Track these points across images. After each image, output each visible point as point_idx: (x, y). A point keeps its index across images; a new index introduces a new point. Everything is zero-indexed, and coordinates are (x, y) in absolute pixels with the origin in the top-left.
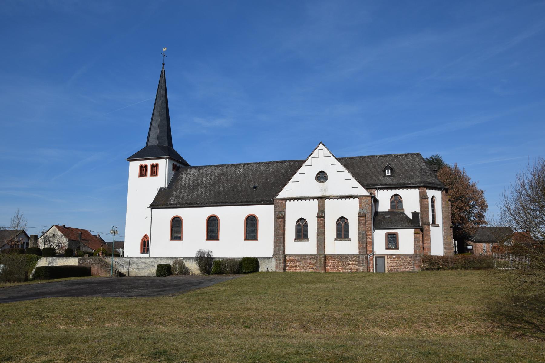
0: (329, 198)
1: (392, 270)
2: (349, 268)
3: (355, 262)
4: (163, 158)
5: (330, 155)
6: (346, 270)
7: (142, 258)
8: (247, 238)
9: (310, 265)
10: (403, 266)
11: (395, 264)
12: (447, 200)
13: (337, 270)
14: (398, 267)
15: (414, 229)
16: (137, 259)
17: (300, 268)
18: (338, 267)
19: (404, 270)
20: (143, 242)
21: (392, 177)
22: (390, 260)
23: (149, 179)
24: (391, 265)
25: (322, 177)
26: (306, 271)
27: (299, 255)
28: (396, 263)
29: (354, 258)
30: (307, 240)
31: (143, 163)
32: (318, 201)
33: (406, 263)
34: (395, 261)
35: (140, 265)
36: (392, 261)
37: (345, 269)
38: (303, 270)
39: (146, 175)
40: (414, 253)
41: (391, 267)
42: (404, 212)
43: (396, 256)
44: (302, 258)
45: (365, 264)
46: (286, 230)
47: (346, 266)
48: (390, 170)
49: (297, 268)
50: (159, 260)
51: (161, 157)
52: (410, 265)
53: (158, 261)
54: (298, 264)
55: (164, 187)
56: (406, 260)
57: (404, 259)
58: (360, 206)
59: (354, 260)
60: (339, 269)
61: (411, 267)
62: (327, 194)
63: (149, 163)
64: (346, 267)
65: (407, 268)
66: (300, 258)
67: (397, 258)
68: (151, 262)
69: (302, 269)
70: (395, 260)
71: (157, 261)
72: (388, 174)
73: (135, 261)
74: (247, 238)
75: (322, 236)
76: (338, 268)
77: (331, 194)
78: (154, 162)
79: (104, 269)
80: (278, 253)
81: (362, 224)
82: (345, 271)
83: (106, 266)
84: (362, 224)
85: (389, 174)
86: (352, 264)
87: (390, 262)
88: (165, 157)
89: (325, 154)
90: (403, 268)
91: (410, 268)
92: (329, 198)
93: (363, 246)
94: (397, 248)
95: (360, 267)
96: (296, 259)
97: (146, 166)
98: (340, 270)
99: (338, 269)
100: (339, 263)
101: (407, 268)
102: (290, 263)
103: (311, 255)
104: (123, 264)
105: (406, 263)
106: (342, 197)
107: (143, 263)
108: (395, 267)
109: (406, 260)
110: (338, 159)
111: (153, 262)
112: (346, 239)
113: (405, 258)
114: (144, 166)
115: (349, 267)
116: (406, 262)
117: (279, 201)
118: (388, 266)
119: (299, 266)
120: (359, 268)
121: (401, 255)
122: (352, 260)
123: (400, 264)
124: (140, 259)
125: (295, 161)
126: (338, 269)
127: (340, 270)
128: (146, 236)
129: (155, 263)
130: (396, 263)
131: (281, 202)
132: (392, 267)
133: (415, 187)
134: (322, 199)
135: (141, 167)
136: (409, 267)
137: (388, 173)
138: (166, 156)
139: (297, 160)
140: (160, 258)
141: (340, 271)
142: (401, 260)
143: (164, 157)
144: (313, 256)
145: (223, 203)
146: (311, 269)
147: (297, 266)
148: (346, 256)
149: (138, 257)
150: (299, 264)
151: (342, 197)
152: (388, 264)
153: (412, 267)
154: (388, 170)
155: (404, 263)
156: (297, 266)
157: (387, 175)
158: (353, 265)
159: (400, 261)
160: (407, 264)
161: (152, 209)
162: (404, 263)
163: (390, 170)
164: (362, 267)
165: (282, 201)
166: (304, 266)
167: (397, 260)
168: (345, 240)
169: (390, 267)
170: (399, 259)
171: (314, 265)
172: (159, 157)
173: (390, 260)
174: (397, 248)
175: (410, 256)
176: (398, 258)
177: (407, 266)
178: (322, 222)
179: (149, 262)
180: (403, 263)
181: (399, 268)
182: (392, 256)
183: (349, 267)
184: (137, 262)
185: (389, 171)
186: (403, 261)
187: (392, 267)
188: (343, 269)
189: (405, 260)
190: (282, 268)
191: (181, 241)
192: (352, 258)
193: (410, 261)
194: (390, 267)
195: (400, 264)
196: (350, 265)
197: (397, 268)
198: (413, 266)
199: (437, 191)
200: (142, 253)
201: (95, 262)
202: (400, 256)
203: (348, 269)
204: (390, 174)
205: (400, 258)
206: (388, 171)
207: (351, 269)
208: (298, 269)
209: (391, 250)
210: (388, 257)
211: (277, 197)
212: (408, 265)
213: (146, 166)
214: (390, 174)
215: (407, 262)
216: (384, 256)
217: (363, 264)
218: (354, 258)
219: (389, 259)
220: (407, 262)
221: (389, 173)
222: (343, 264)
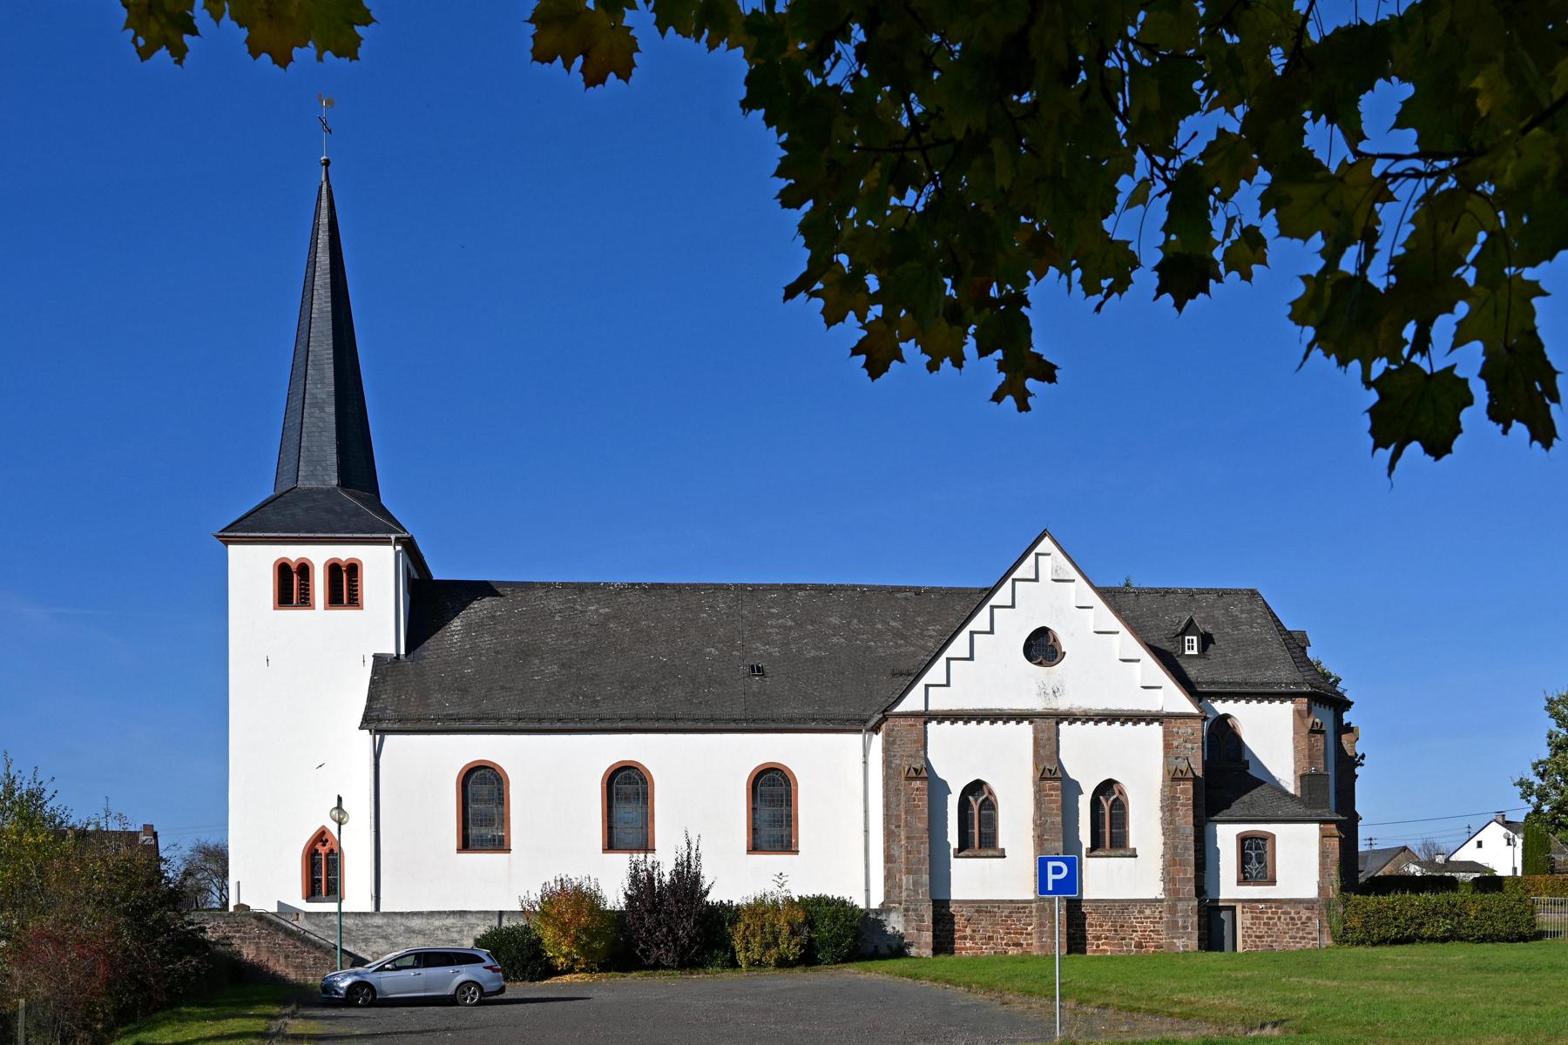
0: (1071, 717)
1: (1257, 946)
2: (1133, 942)
3: (1151, 922)
4: (386, 542)
5: (1074, 574)
6: (1125, 948)
7: (408, 913)
8: (466, 844)
9: (1010, 933)
10: (1287, 936)
11: (1264, 929)
12: (1307, 732)
13: (1094, 947)
14: (1273, 936)
15: (1321, 822)
16: (385, 920)
17: (977, 944)
18: (1098, 938)
19: (1291, 947)
20: (309, 855)
21: (1203, 662)
22: (1249, 915)
23: (319, 617)
24: (1254, 932)
25: (1041, 647)
26: (995, 953)
27: (973, 901)
28: (1268, 924)
29: (1148, 912)
30: (997, 854)
31: (294, 553)
32: (1031, 726)
33: (1297, 924)
34: (1265, 921)
35: (400, 940)
36: (1257, 918)
37: (1121, 946)
38: (987, 950)
39: (305, 601)
40: (1319, 894)
41: (1254, 938)
42: (1248, 771)
43: (1268, 905)
44: (982, 911)
45: (1192, 929)
46: (1158, 814)
47: (1122, 935)
48: (1195, 638)
49: (968, 945)
50: (479, 922)
51: (266, 535)
52: (1308, 930)
53: (472, 927)
54: (968, 931)
55: (391, 650)
56: (1296, 916)
57: (1289, 913)
58: (1167, 746)
59: (1149, 918)
60: (1103, 944)
61: (1310, 936)
62: (1062, 704)
63: (319, 556)
64: (1123, 939)
65: (1298, 940)
66: (977, 911)
67: (1269, 911)
68: (448, 929)
69: (984, 947)
70: (1265, 916)
71: (469, 925)
72: (1189, 649)
73: (377, 927)
74: (466, 844)
75: (1058, 840)
76: (1100, 942)
77: (1093, 708)
78: (344, 553)
79: (287, 957)
80: (912, 893)
81: (1182, 805)
82: (1120, 951)
83: (296, 947)
84: (1182, 805)
85: (1193, 649)
86: (1140, 927)
87: (1252, 924)
88: (393, 537)
89: (1056, 571)
90: (1288, 939)
91: (1309, 939)
92: (1071, 717)
93: (1185, 872)
94: (1273, 882)
95: (1179, 938)
96: (963, 915)
97: (304, 569)
98: (1105, 947)
99: (1098, 946)
100: (1101, 926)
101: (1298, 940)
102: (944, 927)
103: (1011, 901)
104: (329, 936)
105: (1297, 924)
106: (1111, 717)
107: (414, 932)
108: (1266, 939)
109: (1296, 916)
110: (1107, 594)
111: (454, 930)
112: (990, 852)
113: (1293, 912)
114: (294, 568)
115: (1131, 939)
116: (1296, 922)
117: (902, 721)
118: (1244, 936)
119: (972, 938)
120: (1175, 940)
121: (1281, 900)
122: (1142, 916)
123: (1278, 929)
124: (399, 920)
125: (861, 586)
126: (1098, 946)
127: (1105, 947)
128: (321, 836)
129: (460, 931)
130: (1268, 924)
131: (910, 725)
132: (1257, 937)
133: (1283, 696)
134: (1047, 723)
135: (283, 570)
136: (1304, 938)
137: (1189, 646)
138: (399, 535)
139: (870, 586)
140: (482, 916)
141: (1106, 951)
142: (1283, 917)
143: (389, 535)
144: (1021, 905)
145: (852, 724)
146: (1014, 945)
147: (965, 938)
148: (1123, 906)
149: (487, 912)
150: (974, 931)
151: (1111, 717)
152: (1243, 928)
153: (1317, 937)
154: (1190, 638)
155: (1290, 926)
156: (965, 938)
157: (1187, 652)
158: (1145, 931)
159: (1279, 918)
160: (1298, 929)
161: (383, 732)
162: (1290, 926)
163: (1195, 638)
164: (1183, 938)
165: (911, 721)
166: (990, 938)
167: (1270, 915)
168: (1113, 854)
169: (1250, 936)
170: (1276, 913)
171: (1022, 934)
172: (261, 535)
173: (1249, 915)
174: (1273, 882)
175: (1308, 904)
176: (1273, 910)
177: (1301, 934)
178: (1056, 795)
179: (437, 929)
180: (1287, 924)
181: (1276, 941)
182: (1257, 904)
183: (1131, 939)
184: (390, 930)
185: (1192, 640)
186: (1288, 920)
187: (1257, 937)
188: (1114, 945)
189: (1293, 915)
190: (926, 943)
191: (506, 855)
192: (1141, 912)
193: (1309, 919)
194: (1250, 936)
195: (1278, 929)
196: (1135, 934)
197: (1272, 942)
198: (1316, 934)
199: (1151, 709)
200: (1240, 883)
201: (239, 931)
202: (1279, 903)
203: (1129, 945)
204: (1195, 652)
205: (1280, 911)
206: (1189, 640)
207: (1139, 945)
208: (971, 948)
209: (1254, 885)
210: (1244, 907)
211: (899, 709)
212: (1303, 930)
213: (304, 569)
214: (1195, 652)
215: (1299, 922)
216: (1233, 904)
217: (1185, 928)
218: (1148, 912)
219: (1247, 912)
220: (1299, 922)
221: (1189, 642)
222: (1115, 931)
